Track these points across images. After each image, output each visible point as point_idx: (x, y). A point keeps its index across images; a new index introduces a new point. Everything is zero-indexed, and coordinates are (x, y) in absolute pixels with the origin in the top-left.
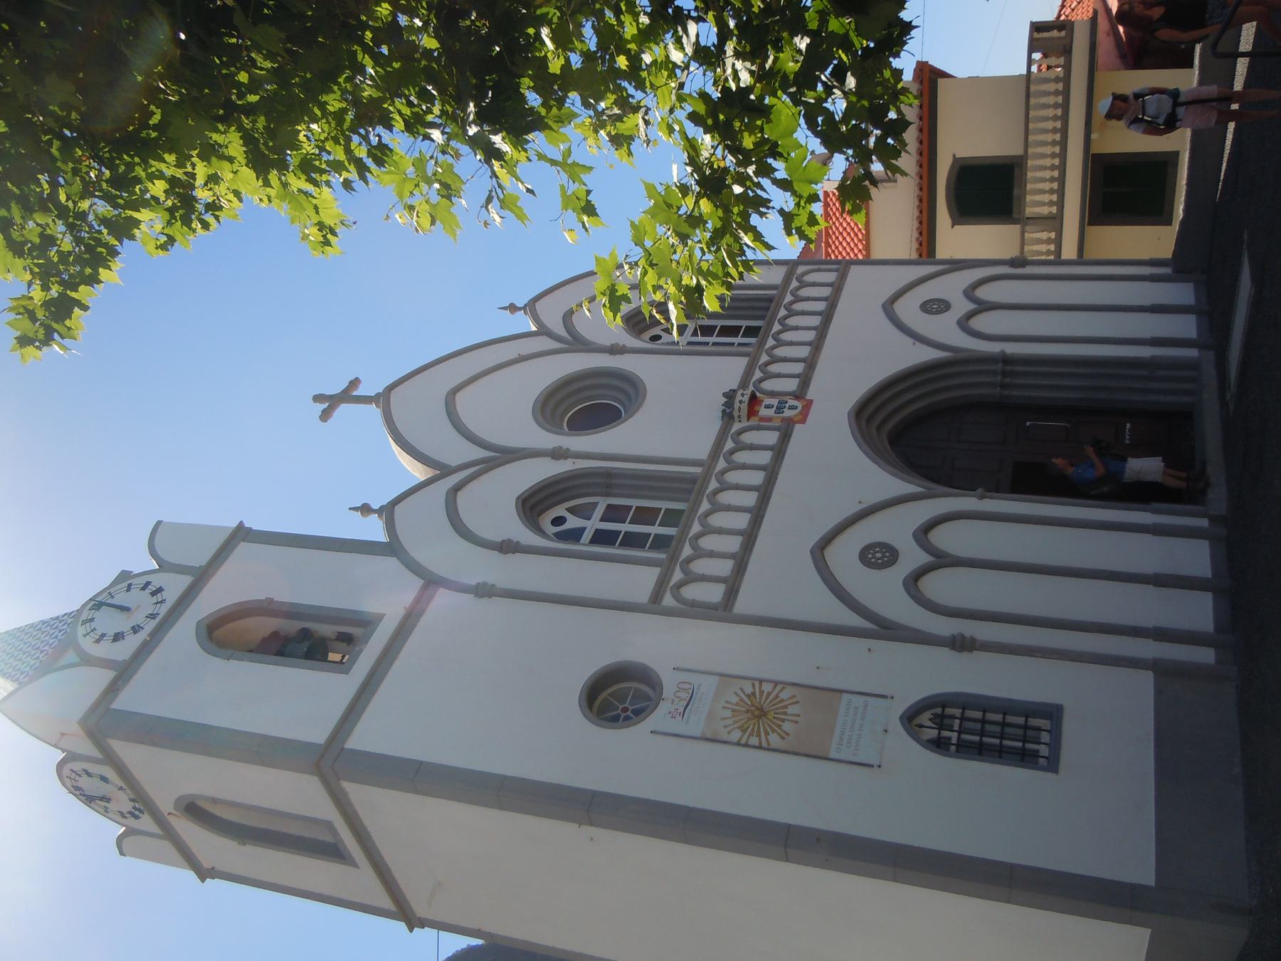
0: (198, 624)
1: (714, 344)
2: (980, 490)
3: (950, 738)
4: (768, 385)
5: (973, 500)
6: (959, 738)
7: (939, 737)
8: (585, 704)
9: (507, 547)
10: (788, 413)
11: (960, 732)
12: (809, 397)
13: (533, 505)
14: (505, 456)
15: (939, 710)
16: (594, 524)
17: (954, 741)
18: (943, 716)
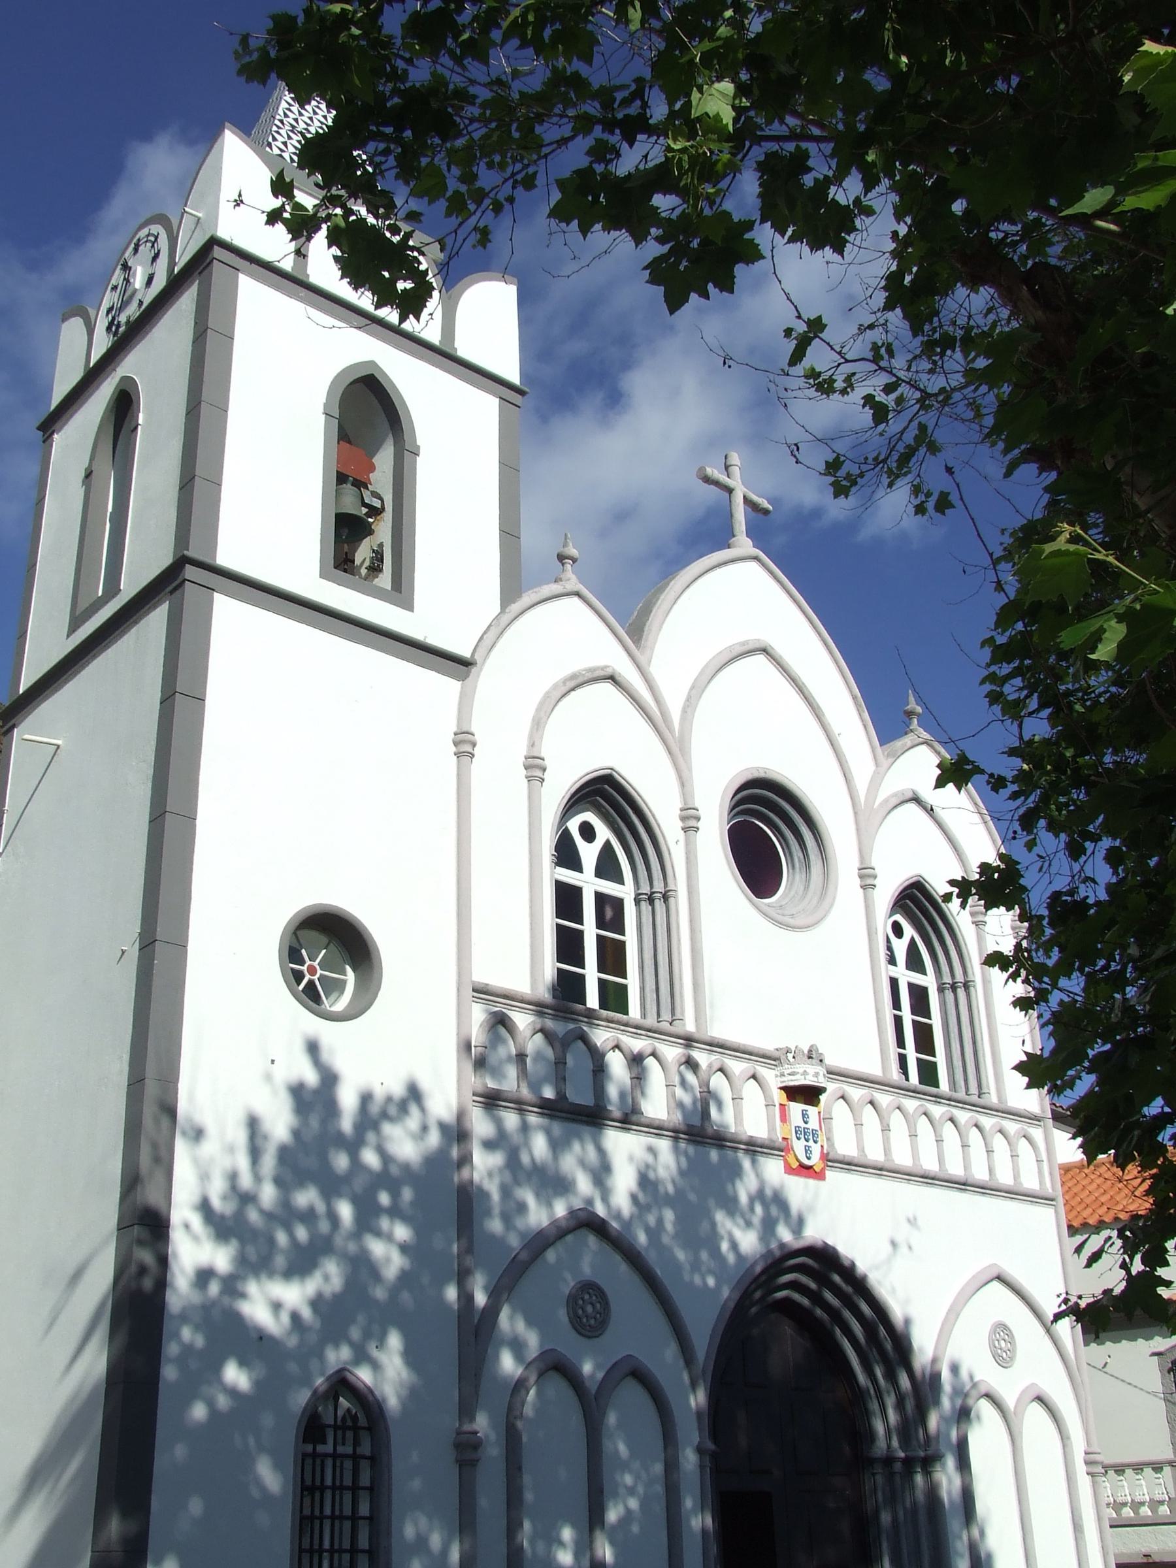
0: (372, 363)
1: (898, 1021)
2: (710, 1446)
3: (324, 1442)
4: (840, 1111)
5: (696, 1439)
6: (326, 1455)
7: (323, 1427)
8: (301, 918)
9: (535, 767)
10: (799, 1146)
11: (335, 1456)
12: (829, 1174)
13: (604, 794)
14: (676, 748)
15: (362, 1421)
16: (589, 883)
17: (321, 1448)
18: (356, 1428)
